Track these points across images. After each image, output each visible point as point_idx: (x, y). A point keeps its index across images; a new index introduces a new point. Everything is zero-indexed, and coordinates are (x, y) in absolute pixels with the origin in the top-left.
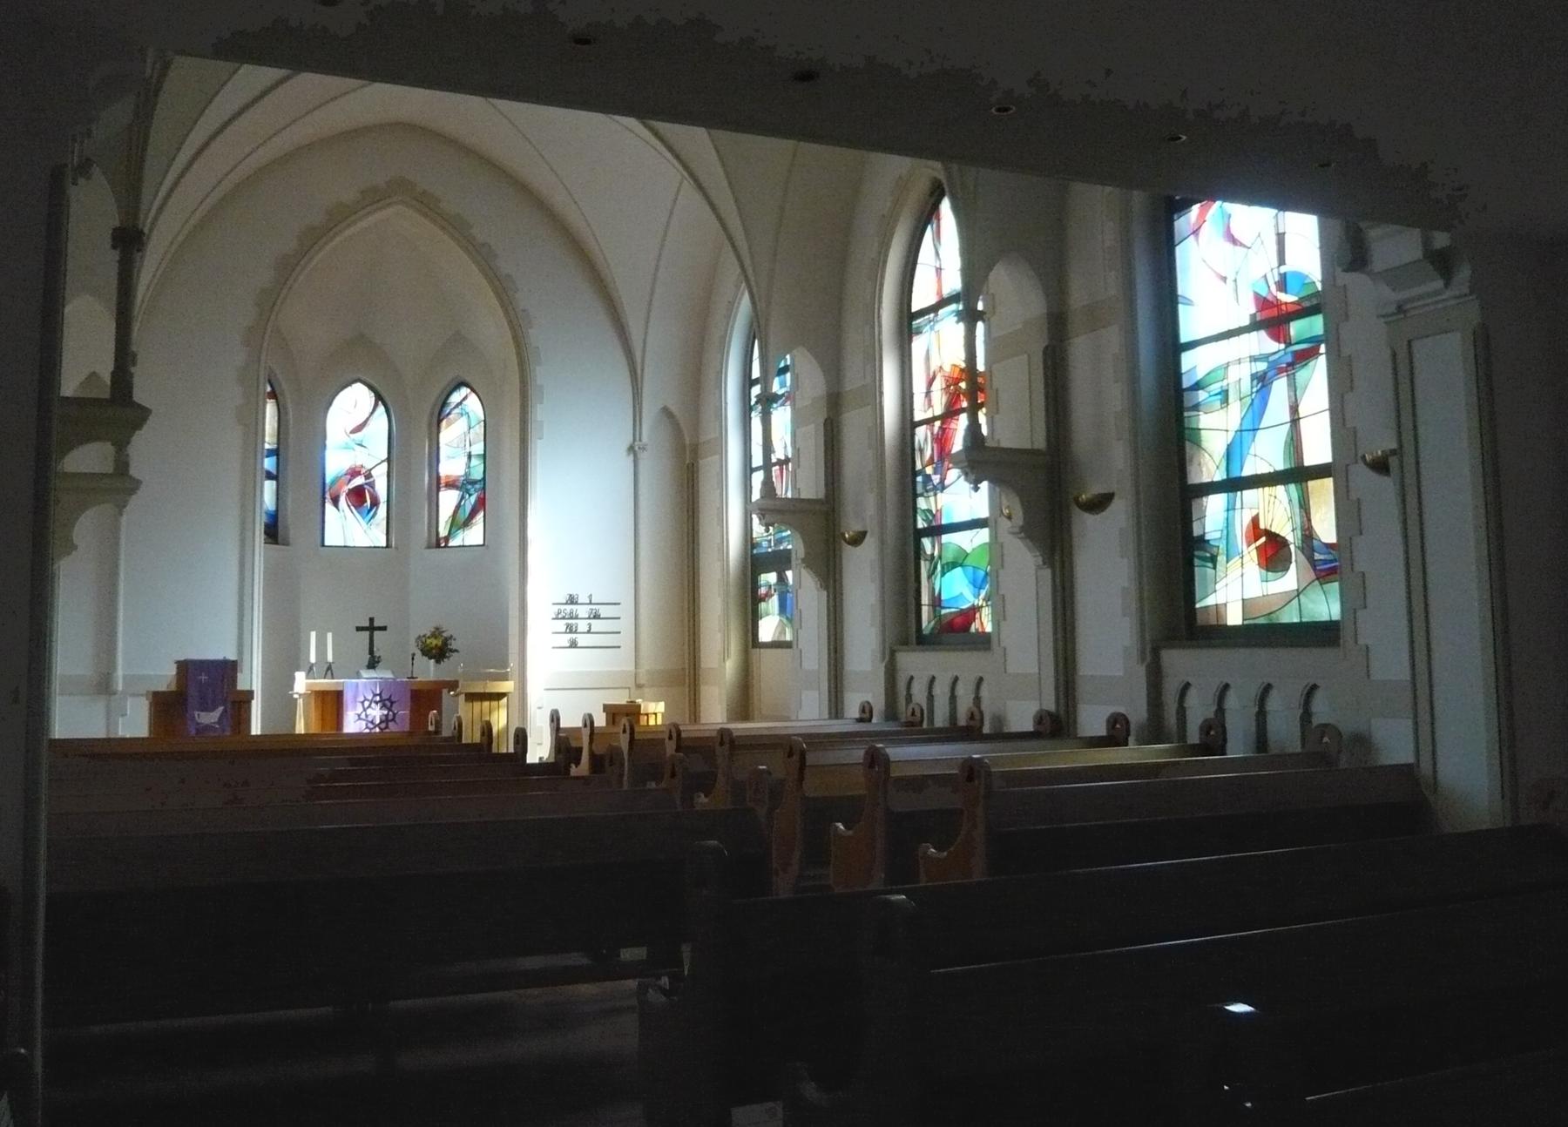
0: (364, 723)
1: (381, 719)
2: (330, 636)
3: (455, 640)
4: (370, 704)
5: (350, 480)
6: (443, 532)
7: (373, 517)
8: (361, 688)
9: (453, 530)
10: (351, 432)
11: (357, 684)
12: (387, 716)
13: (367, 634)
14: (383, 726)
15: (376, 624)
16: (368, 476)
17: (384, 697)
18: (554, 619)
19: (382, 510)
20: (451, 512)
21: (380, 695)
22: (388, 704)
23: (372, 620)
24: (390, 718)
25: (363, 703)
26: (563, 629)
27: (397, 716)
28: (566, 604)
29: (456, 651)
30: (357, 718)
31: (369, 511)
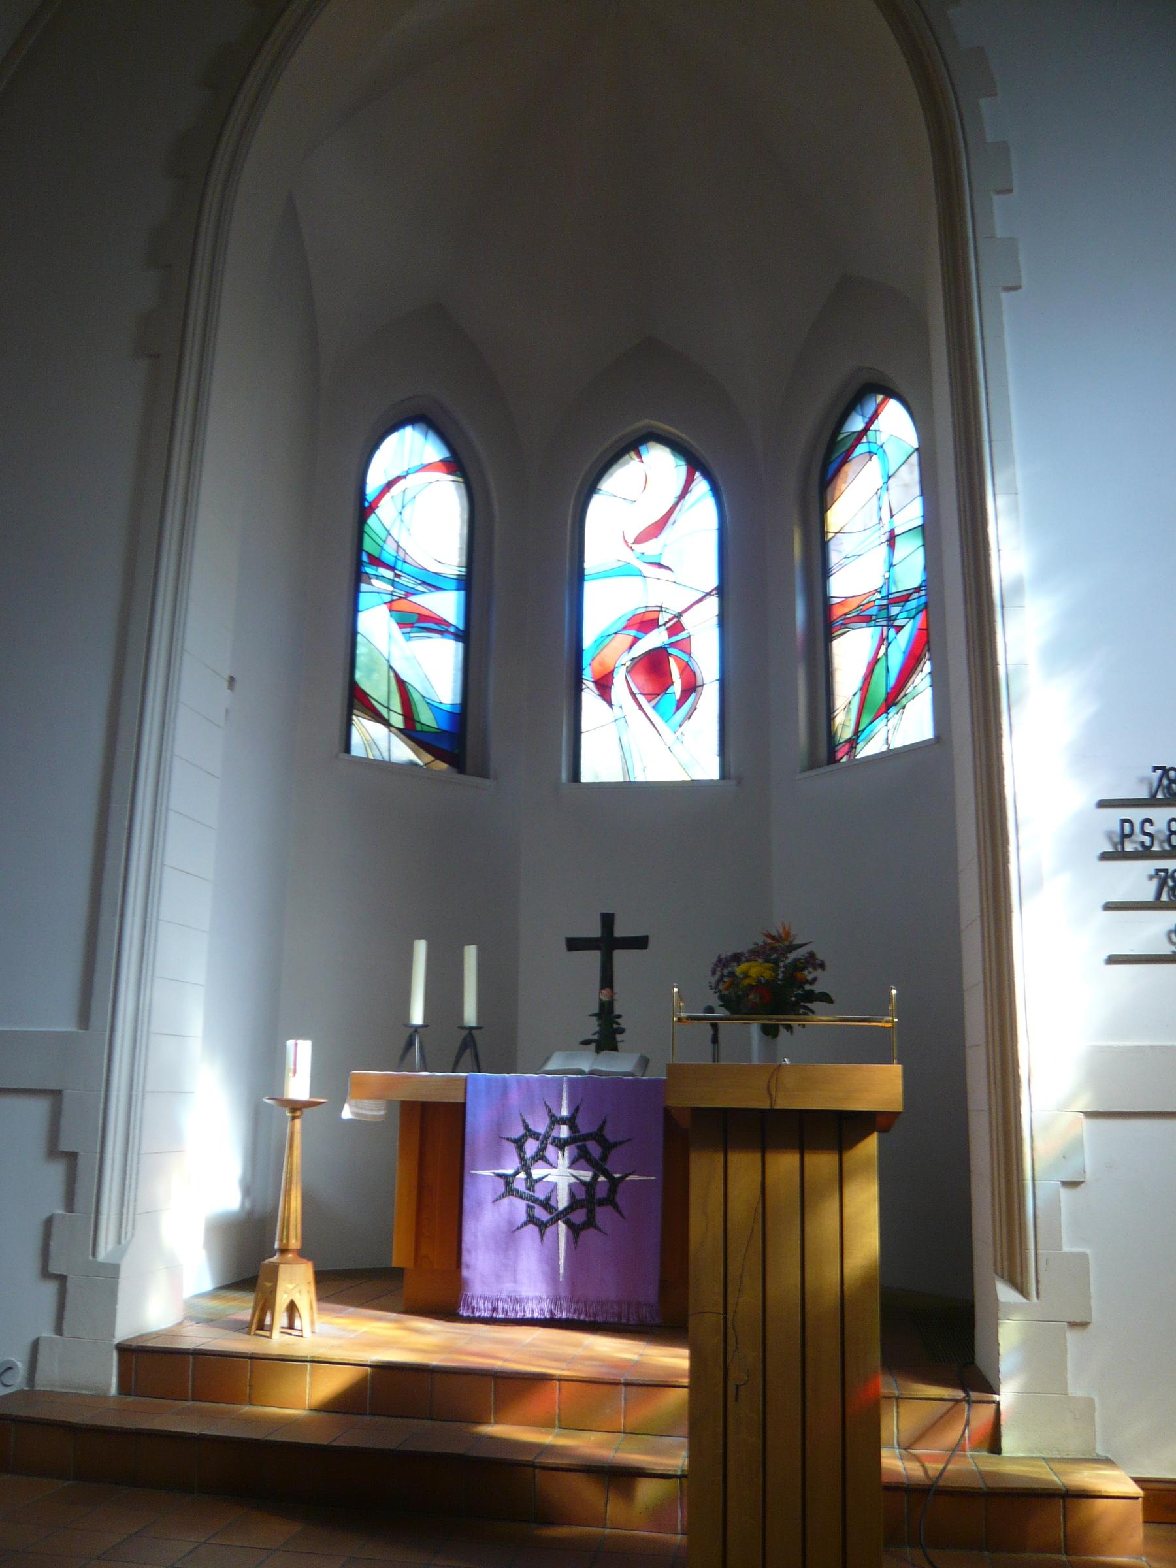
0: (521, 1206)
1: (572, 1195)
2: (471, 954)
3: (822, 966)
4: (542, 1149)
5: (636, 640)
6: (844, 722)
7: (689, 716)
8: (515, 1098)
9: (865, 720)
10: (639, 540)
11: (505, 1085)
12: (590, 1186)
13: (594, 957)
14: (579, 1217)
15: (619, 932)
16: (676, 628)
17: (584, 1128)
18: (1105, 857)
19: (709, 700)
20: (857, 683)
21: (570, 1121)
22: (594, 1149)
23: (608, 921)
24: (601, 1193)
25: (519, 1143)
26: (1147, 892)
27: (620, 1189)
28: (1152, 802)
29: (825, 998)
30: (502, 1189)
31: (680, 704)
